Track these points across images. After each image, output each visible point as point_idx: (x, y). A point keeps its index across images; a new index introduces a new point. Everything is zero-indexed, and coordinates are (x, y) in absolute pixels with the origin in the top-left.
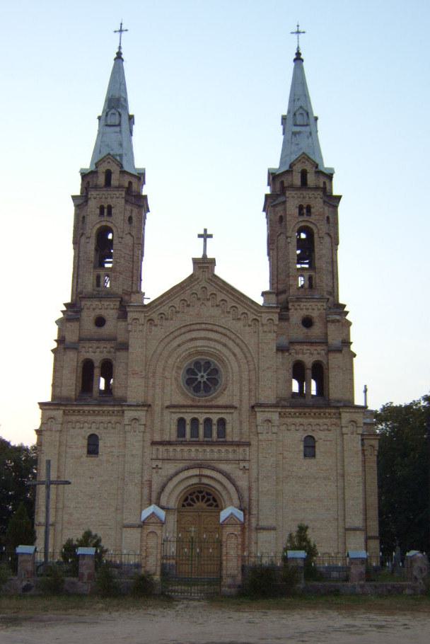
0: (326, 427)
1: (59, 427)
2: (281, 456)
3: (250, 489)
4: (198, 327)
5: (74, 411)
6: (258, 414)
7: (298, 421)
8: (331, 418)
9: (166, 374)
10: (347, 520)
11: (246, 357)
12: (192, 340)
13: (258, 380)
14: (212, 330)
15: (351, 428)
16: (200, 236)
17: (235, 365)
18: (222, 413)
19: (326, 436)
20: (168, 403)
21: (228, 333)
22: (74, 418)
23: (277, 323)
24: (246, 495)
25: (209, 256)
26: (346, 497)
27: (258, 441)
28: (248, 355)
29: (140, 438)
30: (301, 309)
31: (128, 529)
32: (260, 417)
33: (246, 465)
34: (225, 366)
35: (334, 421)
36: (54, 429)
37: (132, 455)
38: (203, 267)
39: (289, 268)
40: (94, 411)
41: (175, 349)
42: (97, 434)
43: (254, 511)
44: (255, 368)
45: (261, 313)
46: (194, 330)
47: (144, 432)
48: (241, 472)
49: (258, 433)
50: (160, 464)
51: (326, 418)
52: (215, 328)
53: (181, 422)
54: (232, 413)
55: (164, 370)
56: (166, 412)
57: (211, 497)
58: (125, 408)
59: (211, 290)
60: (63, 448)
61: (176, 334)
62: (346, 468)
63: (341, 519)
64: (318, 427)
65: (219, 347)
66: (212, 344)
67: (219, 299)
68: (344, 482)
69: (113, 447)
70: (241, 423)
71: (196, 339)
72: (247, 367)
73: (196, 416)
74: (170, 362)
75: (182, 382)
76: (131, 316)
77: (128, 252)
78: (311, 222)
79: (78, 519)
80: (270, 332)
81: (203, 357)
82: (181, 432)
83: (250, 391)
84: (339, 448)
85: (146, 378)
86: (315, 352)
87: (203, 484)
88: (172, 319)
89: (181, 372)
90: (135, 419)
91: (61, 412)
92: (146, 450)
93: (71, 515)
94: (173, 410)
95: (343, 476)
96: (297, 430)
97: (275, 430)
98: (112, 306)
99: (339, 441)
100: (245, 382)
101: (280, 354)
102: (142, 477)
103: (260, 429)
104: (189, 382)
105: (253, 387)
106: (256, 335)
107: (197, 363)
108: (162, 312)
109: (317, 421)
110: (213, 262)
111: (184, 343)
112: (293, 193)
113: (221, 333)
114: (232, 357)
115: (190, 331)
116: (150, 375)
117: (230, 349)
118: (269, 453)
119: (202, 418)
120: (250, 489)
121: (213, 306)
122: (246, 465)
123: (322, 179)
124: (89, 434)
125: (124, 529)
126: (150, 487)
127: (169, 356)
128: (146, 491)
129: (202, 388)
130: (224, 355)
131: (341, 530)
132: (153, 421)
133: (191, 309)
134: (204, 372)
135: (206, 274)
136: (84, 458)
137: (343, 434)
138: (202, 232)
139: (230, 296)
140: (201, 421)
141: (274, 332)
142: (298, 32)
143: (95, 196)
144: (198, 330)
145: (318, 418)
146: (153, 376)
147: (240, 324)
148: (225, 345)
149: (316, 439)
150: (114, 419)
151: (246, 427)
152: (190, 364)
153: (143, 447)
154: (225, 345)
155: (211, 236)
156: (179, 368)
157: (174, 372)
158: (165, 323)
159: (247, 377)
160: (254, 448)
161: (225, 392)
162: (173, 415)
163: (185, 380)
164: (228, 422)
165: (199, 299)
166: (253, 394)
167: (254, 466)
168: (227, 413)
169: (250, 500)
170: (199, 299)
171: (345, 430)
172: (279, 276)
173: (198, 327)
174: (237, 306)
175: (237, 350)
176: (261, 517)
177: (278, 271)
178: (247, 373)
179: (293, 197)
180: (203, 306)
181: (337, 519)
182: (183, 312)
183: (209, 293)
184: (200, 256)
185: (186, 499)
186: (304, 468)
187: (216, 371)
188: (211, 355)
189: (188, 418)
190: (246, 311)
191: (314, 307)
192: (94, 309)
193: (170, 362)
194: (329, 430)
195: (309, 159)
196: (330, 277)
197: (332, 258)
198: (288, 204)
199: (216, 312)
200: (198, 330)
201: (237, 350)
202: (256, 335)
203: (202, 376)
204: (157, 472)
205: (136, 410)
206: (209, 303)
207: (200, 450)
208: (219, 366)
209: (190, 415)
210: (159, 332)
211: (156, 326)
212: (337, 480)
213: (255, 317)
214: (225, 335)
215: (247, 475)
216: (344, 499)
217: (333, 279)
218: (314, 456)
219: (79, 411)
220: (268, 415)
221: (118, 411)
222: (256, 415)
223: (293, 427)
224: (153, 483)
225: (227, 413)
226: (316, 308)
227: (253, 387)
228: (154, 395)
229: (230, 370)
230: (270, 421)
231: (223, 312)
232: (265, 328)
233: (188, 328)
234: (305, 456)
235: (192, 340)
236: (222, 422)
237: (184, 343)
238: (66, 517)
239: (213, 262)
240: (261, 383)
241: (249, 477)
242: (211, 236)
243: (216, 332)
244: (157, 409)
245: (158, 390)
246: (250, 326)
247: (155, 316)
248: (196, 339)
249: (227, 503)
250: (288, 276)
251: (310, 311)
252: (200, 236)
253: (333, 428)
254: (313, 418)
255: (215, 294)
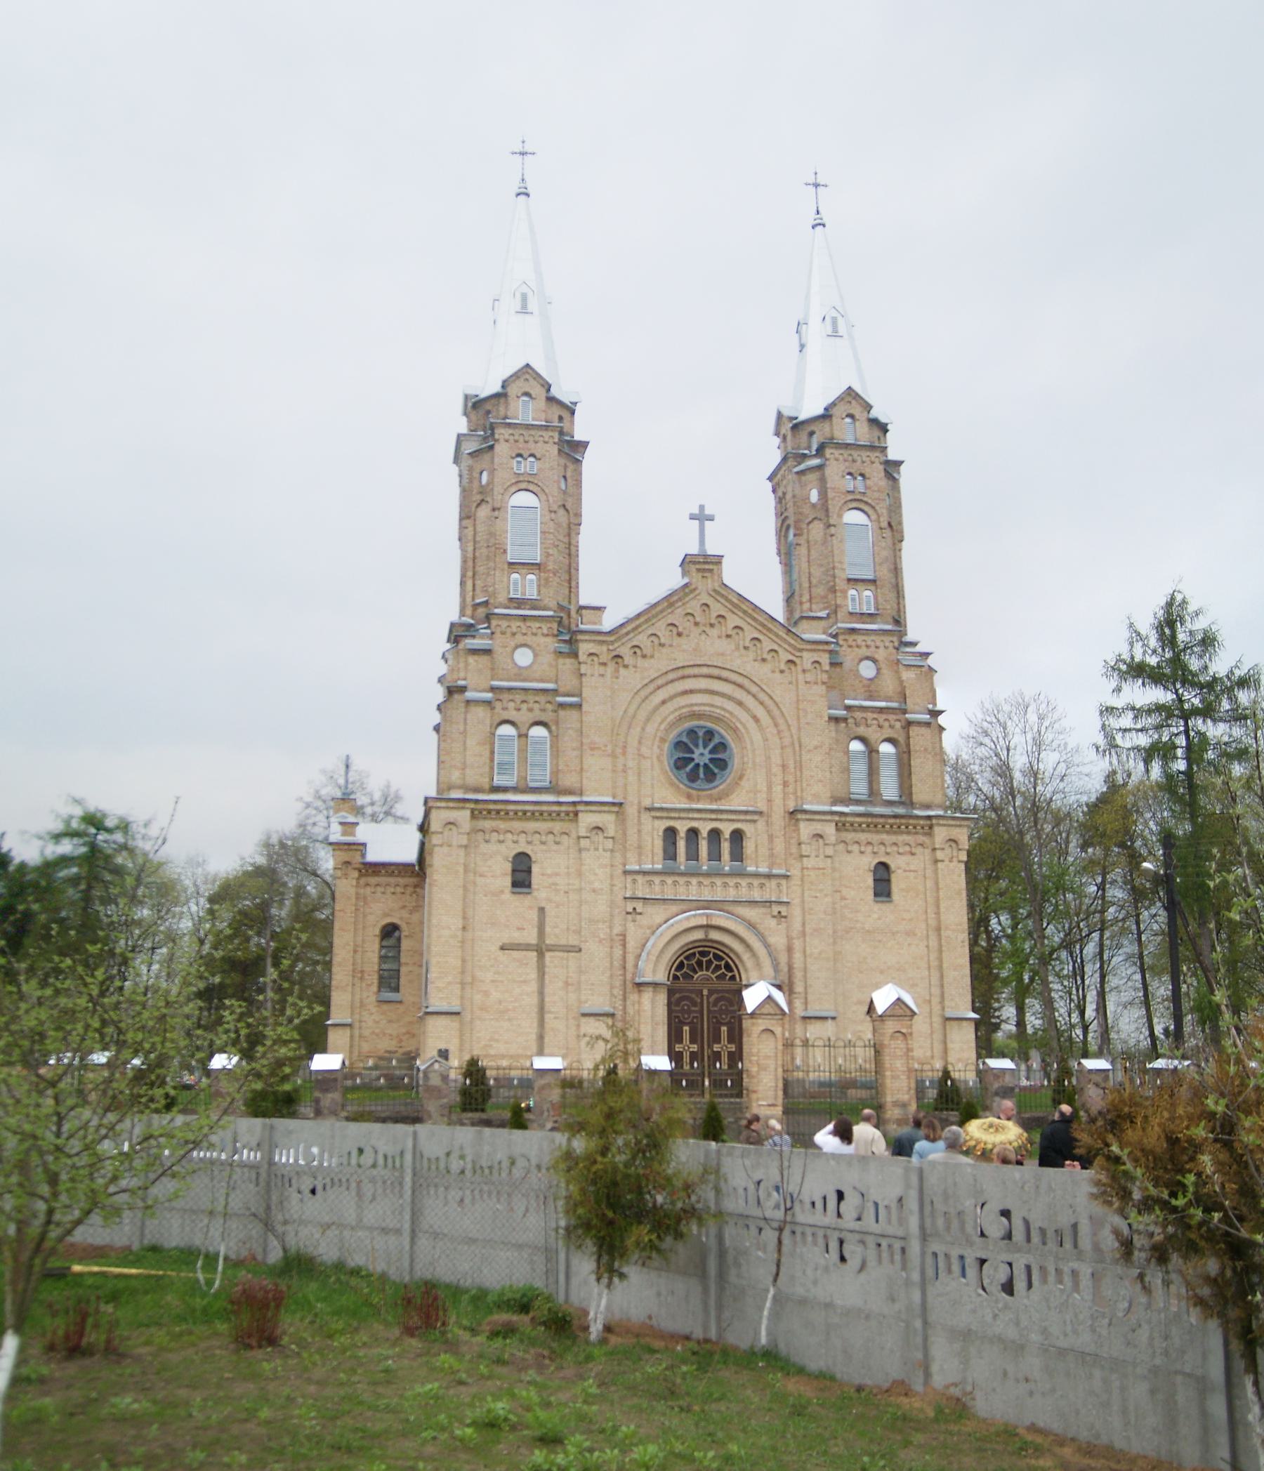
0: (907, 848)
1: (464, 840)
2: (838, 896)
3: (790, 949)
4: (696, 671)
5: (489, 812)
6: (802, 825)
7: (863, 837)
8: (916, 833)
9: (644, 750)
10: (947, 1003)
11: (776, 725)
12: (685, 693)
13: (800, 766)
14: (719, 678)
15: (948, 851)
16: (692, 517)
17: (757, 737)
18: (738, 821)
19: (908, 864)
20: (647, 802)
21: (746, 683)
22: (487, 824)
23: (827, 667)
24: (783, 959)
25: (711, 550)
26: (945, 965)
27: (803, 869)
28: (781, 721)
29: (606, 861)
30: (858, 646)
31: (591, 1020)
32: (806, 829)
33: (783, 910)
34: (739, 738)
35: (921, 838)
36: (455, 843)
37: (594, 891)
38: (704, 570)
39: (834, 576)
40: (525, 812)
41: (656, 709)
42: (529, 852)
43: (799, 988)
44: (793, 744)
45: (801, 650)
46: (689, 677)
47: (612, 851)
48: (773, 922)
49: (802, 856)
50: (639, 906)
51: (909, 833)
52: (725, 674)
53: (671, 833)
54: (755, 821)
55: (640, 742)
56: (646, 817)
57: (723, 963)
58: (580, 808)
59: (717, 609)
60: (471, 876)
61: (660, 682)
62: (943, 917)
63: (935, 1000)
64: (895, 848)
65: (730, 706)
66: (718, 701)
67: (731, 624)
68: (940, 940)
69: (557, 874)
70: (771, 838)
71: (691, 692)
72: (778, 741)
73: (695, 824)
74: (651, 729)
75: (667, 764)
76: (584, 648)
77: (561, 538)
78: (866, 503)
79: (500, 1002)
80: (816, 683)
81: (702, 723)
82: (670, 854)
83: (785, 784)
84: (930, 884)
85: (613, 755)
86: (886, 724)
87: (712, 941)
88: (652, 657)
89: (666, 746)
90: (598, 828)
91: (468, 813)
92: (616, 882)
93: (487, 994)
94: (658, 814)
95: (938, 929)
96: (862, 853)
97: (829, 851)
98: (545, 631)
99: (929, 873)
100: (776, 769)
101: (832, 724)
102: (611, 928)
103: (805, 849)
104: (680, 764)
105: (791, 779)
106: (793, 687)
107: (692, 732)
108: (635, 643)
109: (893, 838)
110: (718, 560)
111: (672, 698)
112: (837, 452)
113: (734, 683)
114: (751, 724)
115: (683, 677)
116: (619, 751)
117: (747, 710)
118: (821, 891)
119: (705, 829)
120: (790, 949)
121: (719, 637)
122: (783, 910)
123: (556, 411)
124: (515, 852)
125: (584, 1020)
126: (624, 946)
127: (648, 720)
128: (618, 952)
129: (702, 775)
130: (738, 720)
131: (937, 1020)
132: (625, 834)
133: (683, 640)
134: (705, 747)
135: (709, 581)
136: (507, 895)
137: (936, 861)
138: (696, 511)
139: (749, 620)
140: (704, 833)
141: (824, 683)
142: (816, 185)
143: (507, 437)
144: (695, 676)
145: (895, 833)
146: (624, 753)
147: (766, 668)
148: (740, 703)
149: (893, 866)
150: (557, 826)
151: (779, 846)
152: (680, 735)
153: (612, 877)
154: (740, 703)
155: (711, 518)
156: (663, 740)
157: (655, 747)
158: (640, 662)
159: (779, 762)
160: (796, 881)
161: (743, 783)
162: (657, 823)
163: (672, 762)
164: (748, 835)
165: (696, 624)
166: (790, 789)
167: (796, 912)
168: (747, 821)
169: (790, 968)
170: (696, 624)
171: (939, 855)
172: (813, 590)
173: (696, 671)
174: (761, 637)
175: (760, 712)
176: (810, 998)
177: (810, 582)
178: (778, 751)
179: (837, 460)
180: (704, 636)
181: (930, 1002)
182: (671, 646)
183: (714, 615)
184: (694, 549)
185: (681, 966)
186: (876, 916)
187: (723, 746)
188: (718, 719)
189: (682, 827)
190: (776, 647)
191: (878, 644)
192: (514, 634)
193: (651, 729)
194: (913, 854)
195: (857, 396)
196: (893, 595)
197: (895, 564)
198: (828, 471)
199: (724, 645)
200: (695, 676)
201: (760, 712)
202: (793, 687)
203: (701, 755)
204: (634, 921)
205: (600, 812)
206: (714, 632)
207: (731, 884)
208: (729, 738)
209: (685, 822)
210: (631, 679)
211: (626, 666)
212: (928, 936)
213: (791, 657)
214: (740, 686)
215: (784, 925)
216: (940, 967)
217: (898, 597)
218: (889, 895)
219: (498, 812)
220: (818, 827)
221: (567, 813)
222: (797, 830)
223: (855, 848)
224: (628, 938)
225: (747, 821)
226: (881, 645)
227: (791, 779)
228: (625, 786)
229: (749, 747)
230: (821, 836)
231: (737, 648)
232: (809, 677)
233: (680, 673)
234: (876, 895)
235: (685, 693)
236: (737, 836)
237: (672, 698)
238: (478, 998)
239: (718, 560)
240: (806, 773)
241: (788, 928)
242: (711, 518)
243: (726, 680)
244: (631, 811)
245: (632, 778)
246: (782, 672)
247: (625, 651)
248: (691, 692)
249: (753, 975)
250: (833, 590)
251: (873, 649)
252: (692, 517)
253: (919, 850)
254: (888, 833)
255: (723, 617)
